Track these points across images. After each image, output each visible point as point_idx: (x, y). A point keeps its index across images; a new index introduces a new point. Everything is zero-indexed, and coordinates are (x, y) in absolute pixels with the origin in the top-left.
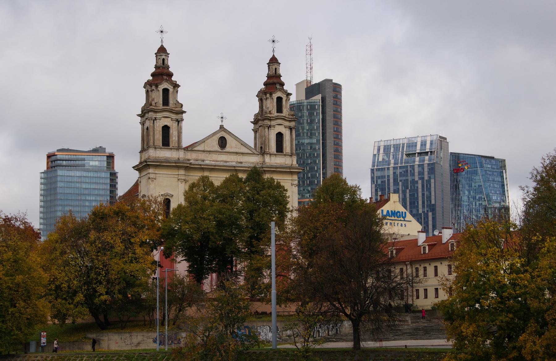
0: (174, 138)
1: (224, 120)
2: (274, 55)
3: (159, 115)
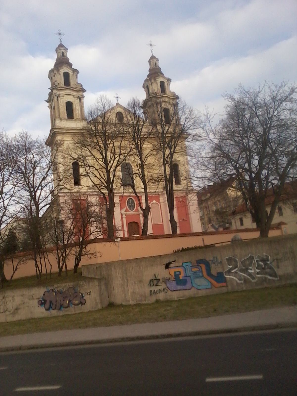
0: (77, 112)
1: (119, 99)
2: (152, 55)
3: (62, 93)
